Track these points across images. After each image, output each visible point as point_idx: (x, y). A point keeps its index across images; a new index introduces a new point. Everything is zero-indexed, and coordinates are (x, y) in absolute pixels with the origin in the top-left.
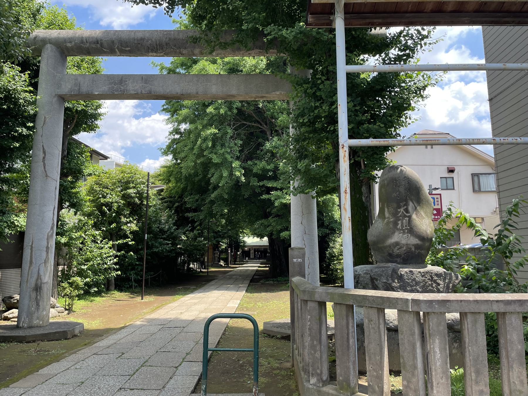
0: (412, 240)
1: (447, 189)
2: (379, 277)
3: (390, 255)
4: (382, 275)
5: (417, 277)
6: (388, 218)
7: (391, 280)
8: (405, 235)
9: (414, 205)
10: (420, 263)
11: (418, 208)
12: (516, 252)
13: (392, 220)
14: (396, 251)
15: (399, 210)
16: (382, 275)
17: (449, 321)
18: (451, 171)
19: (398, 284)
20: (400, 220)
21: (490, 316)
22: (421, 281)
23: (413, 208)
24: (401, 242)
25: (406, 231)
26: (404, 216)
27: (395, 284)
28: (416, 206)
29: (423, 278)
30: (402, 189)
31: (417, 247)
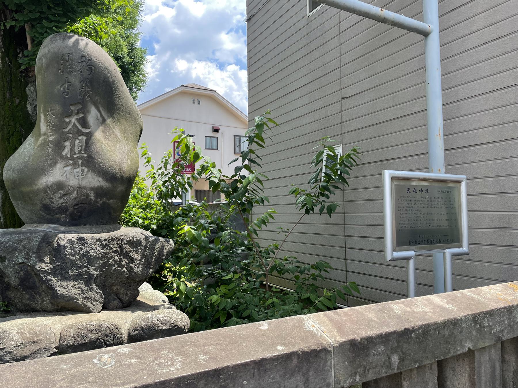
0: (91, 180)
1: (211, 149)
2: (9, 253)
3: (46, 208)
4: (16, 249)
5: (92, 249)
6: (45, 134)
7: (37, 257)
8: (78, 170)
9: (101, 115)
10: (106, 223)
11: (109, 121)
12: (257, 202)
13: (51, 138)
14: (58, 200)
15: (67, 120)
16: (16, 249)
17: (136, 332)
18: (216, 131)
19: (51, 266)
20: (68, 139)
21: (215, 304)
22: (100, 256)
23: (97, 119)
24: (67, 184)
25: (80, 162)
26: (77, 133)
27: (43, 265)
28: (106, 117)
29: (105, 251)
30: (75, 80)
31: (99, 192)
